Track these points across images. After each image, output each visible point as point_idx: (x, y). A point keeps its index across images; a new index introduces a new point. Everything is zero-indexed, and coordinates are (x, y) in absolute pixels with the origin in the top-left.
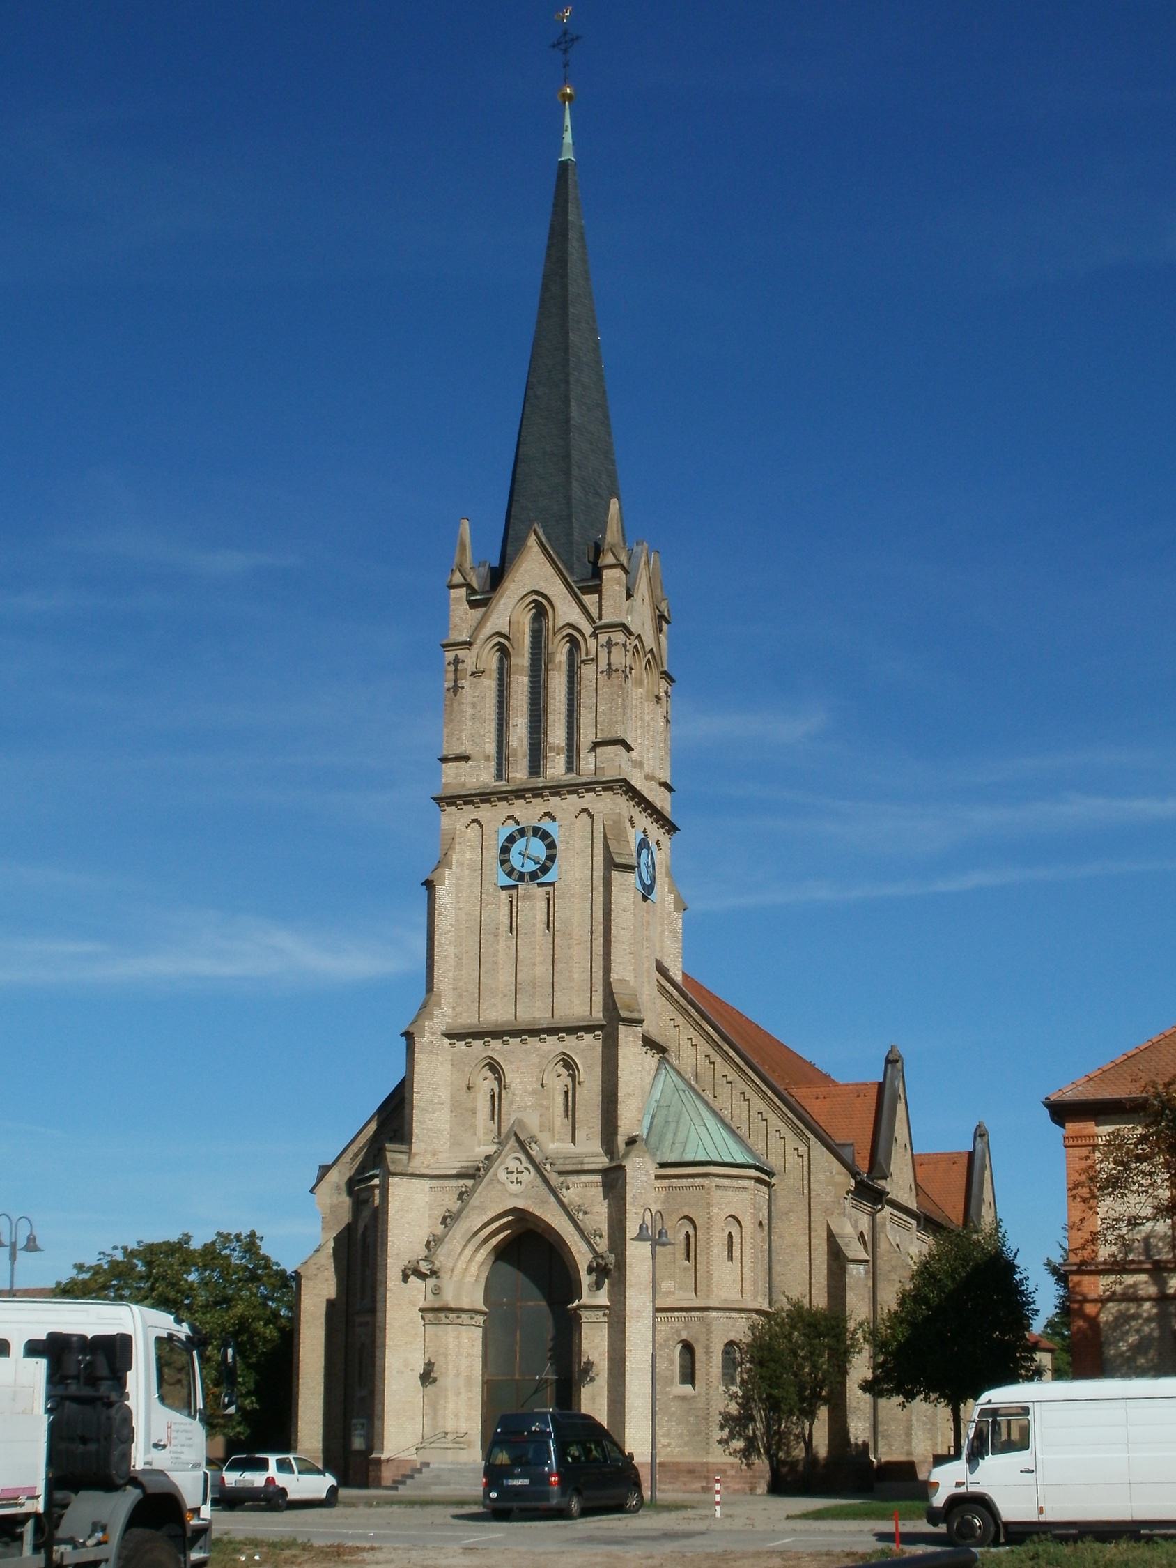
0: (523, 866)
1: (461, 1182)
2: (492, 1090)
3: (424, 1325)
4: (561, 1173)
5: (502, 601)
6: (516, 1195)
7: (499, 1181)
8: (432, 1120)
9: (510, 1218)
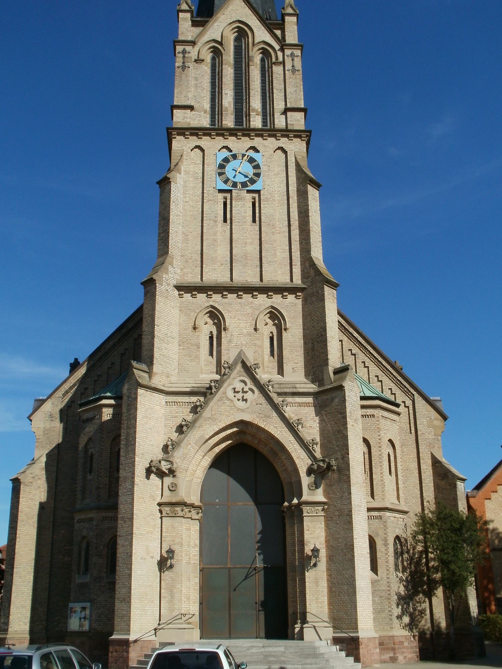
0: (234, 177)
1: (194, 399)
4: (279, 394)
5: (216, 24)
6: (243, 410)
9: (235, 429)
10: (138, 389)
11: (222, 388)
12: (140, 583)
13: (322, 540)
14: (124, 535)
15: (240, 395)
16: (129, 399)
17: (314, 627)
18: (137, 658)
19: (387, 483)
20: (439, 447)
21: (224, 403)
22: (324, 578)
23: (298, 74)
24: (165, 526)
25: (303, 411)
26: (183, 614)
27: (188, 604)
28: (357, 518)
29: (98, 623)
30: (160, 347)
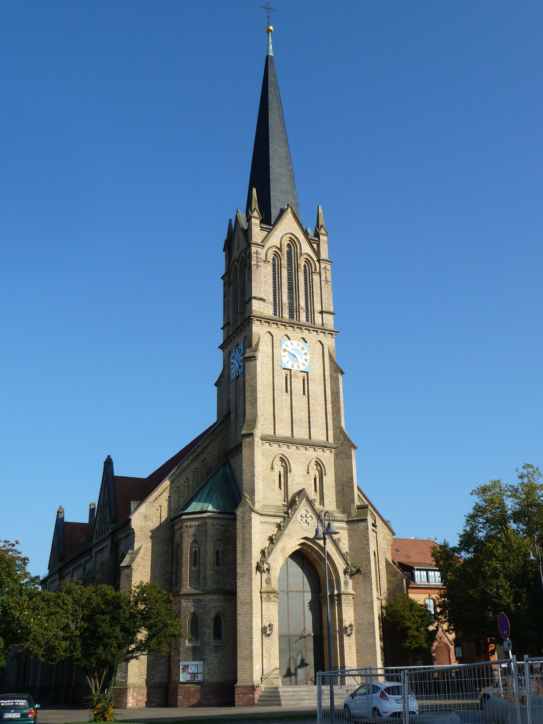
0: (287, 363)
2: (280, 472)
5: (276, 233)
21: (296, 525)
23: (329, 285)
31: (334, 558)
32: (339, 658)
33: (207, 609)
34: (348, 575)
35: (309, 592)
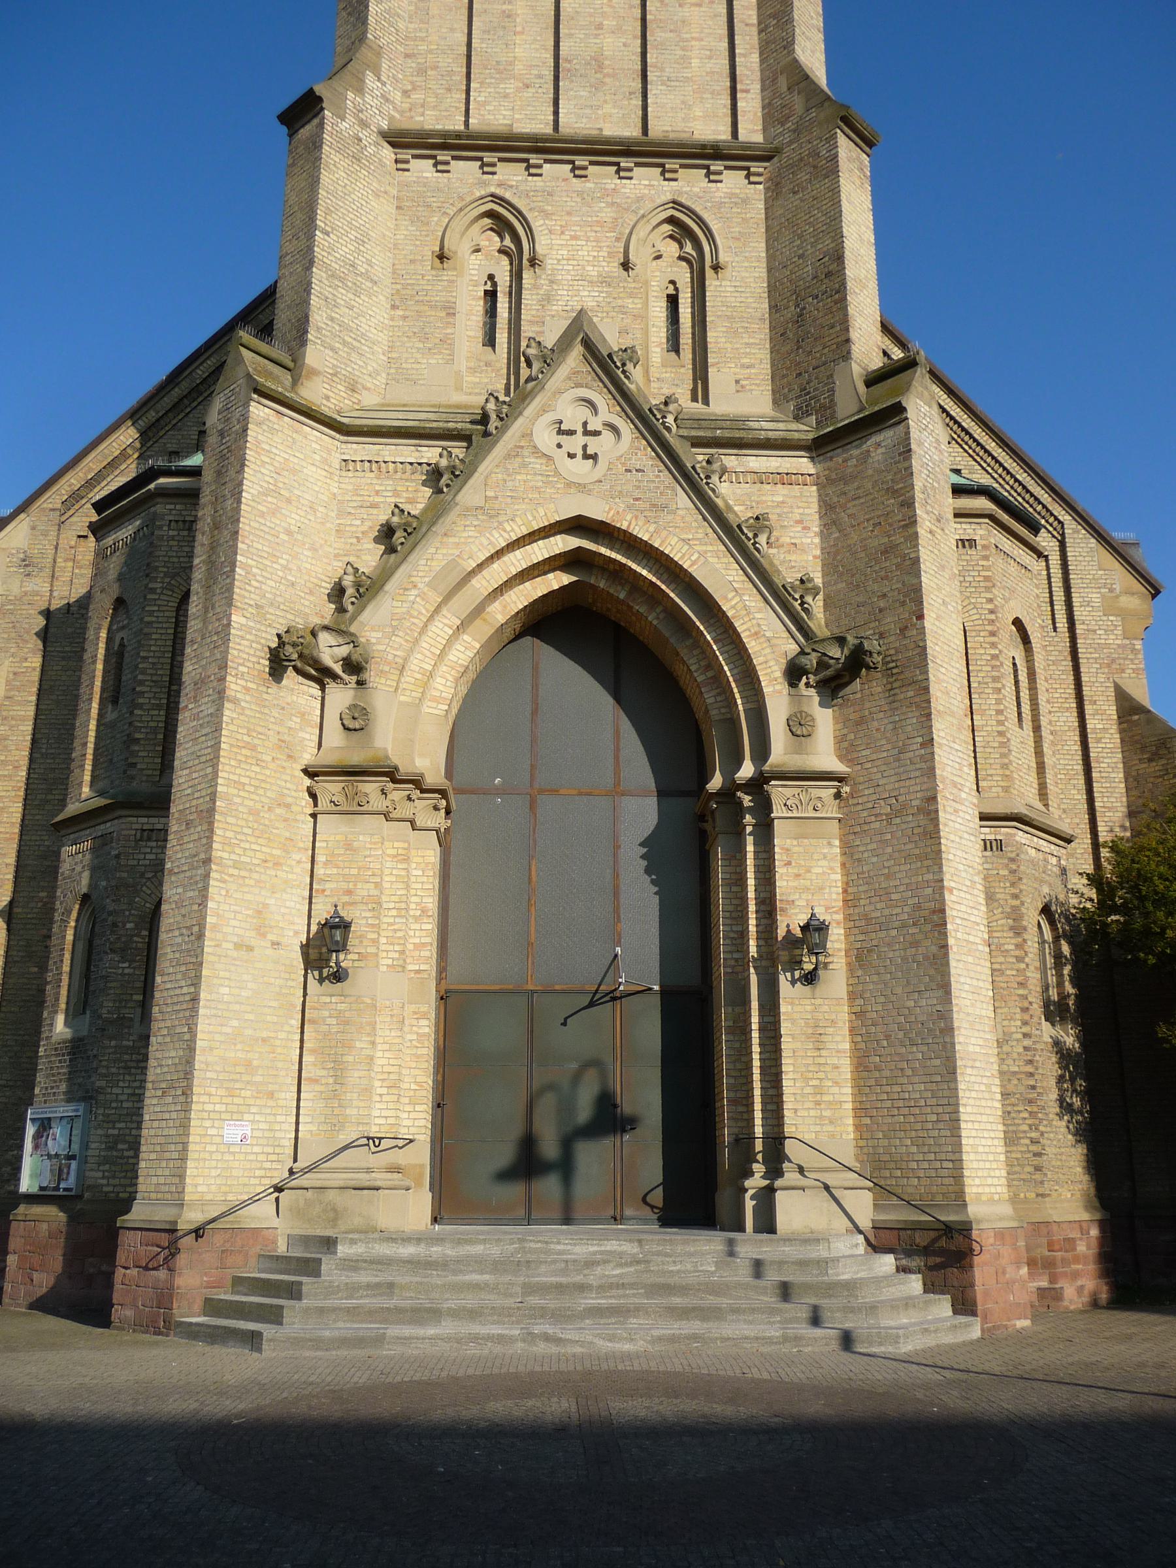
1: (431, 453)
3: (314, 816)
6: (582, 488)
7: (536, 451)
8: (351, 308)
10: (252, 403)
11: (520, 420)
12: (228, 1030)
13: (834, 896)
14: (185, 868)
15: (576, 443)
16: (223, 438)
17: (827, 1188)
18: (204, 1291)
19: (1014, 744)
20: (1138, 669)
21: (524, 465)
22: (840, 1024)
24: (324, 844)
25: (770, 498)
26: (373, 1138)
27: (391, 1106)
28: (951, 823)
29: (107, 1167)
30: (330, 296)
31: (733, 607)
32: (757, 1092)
33: (125, 875)
34: (807, 685)
35: (645, 794)
